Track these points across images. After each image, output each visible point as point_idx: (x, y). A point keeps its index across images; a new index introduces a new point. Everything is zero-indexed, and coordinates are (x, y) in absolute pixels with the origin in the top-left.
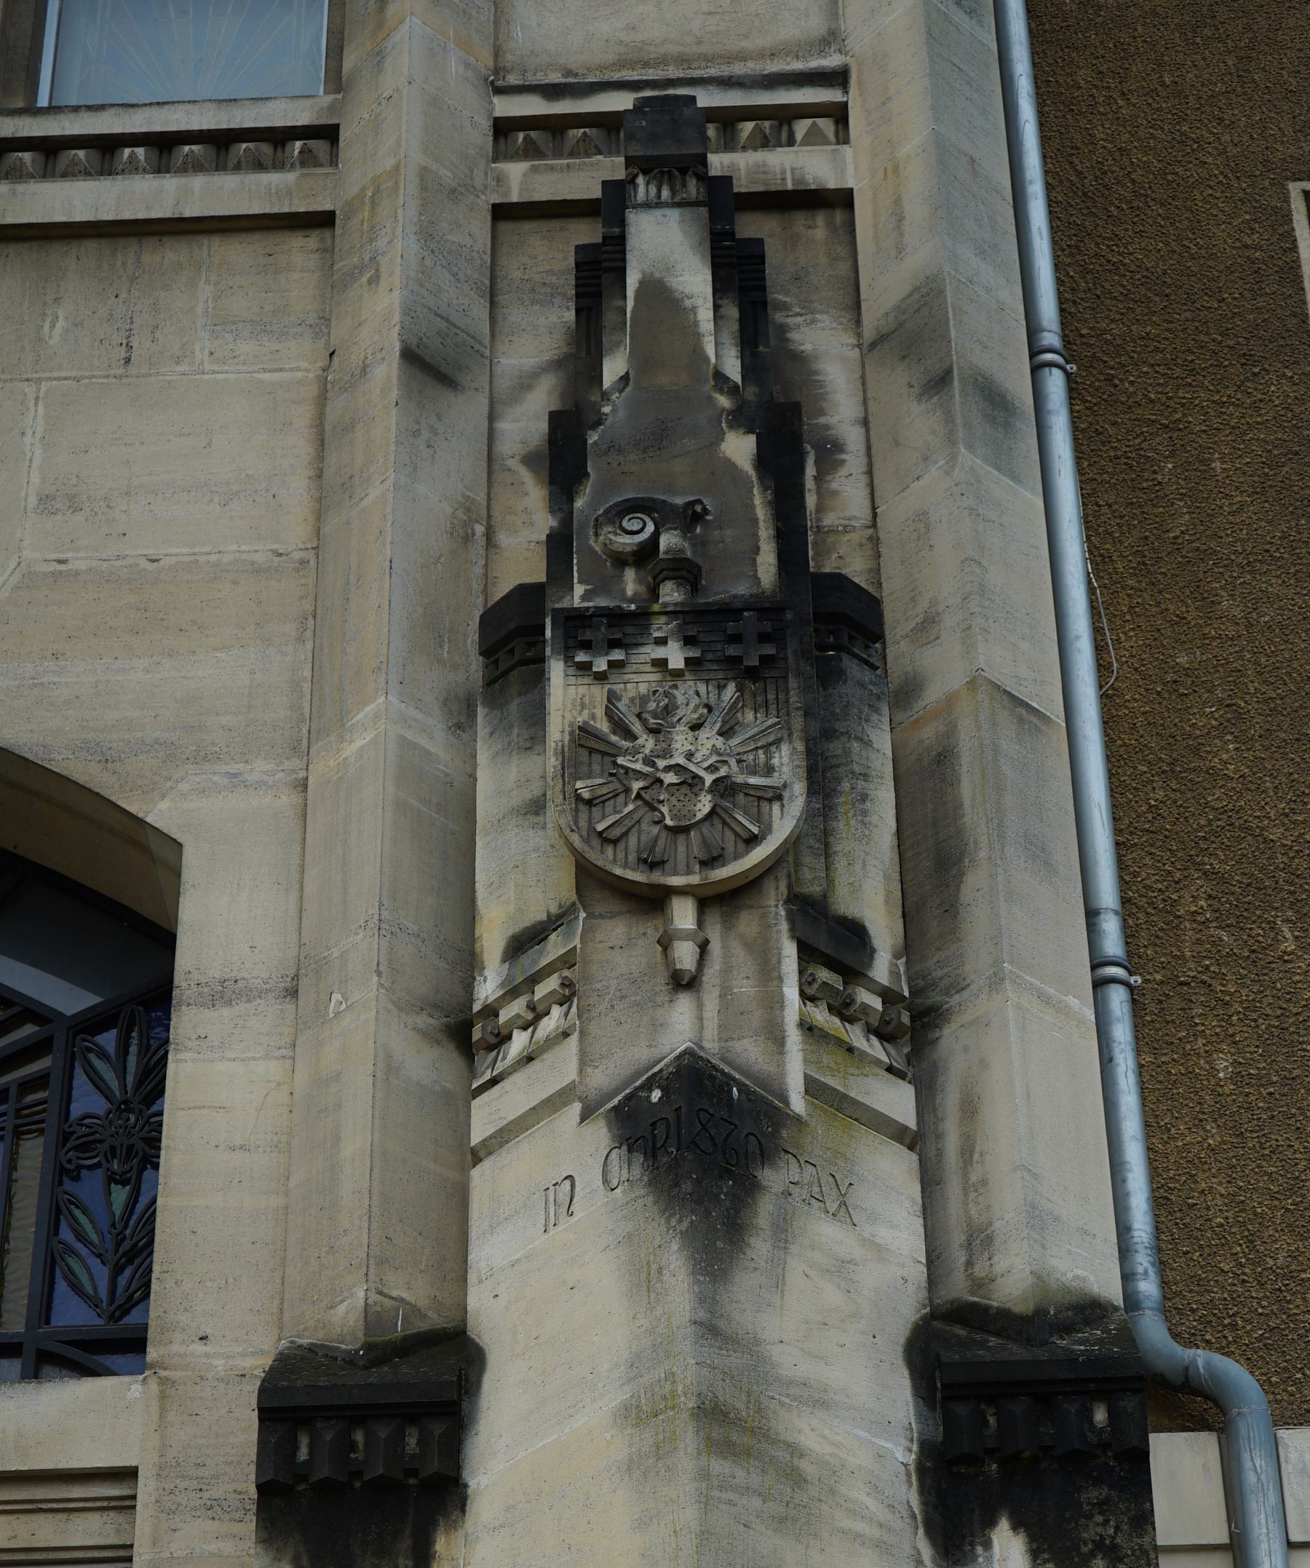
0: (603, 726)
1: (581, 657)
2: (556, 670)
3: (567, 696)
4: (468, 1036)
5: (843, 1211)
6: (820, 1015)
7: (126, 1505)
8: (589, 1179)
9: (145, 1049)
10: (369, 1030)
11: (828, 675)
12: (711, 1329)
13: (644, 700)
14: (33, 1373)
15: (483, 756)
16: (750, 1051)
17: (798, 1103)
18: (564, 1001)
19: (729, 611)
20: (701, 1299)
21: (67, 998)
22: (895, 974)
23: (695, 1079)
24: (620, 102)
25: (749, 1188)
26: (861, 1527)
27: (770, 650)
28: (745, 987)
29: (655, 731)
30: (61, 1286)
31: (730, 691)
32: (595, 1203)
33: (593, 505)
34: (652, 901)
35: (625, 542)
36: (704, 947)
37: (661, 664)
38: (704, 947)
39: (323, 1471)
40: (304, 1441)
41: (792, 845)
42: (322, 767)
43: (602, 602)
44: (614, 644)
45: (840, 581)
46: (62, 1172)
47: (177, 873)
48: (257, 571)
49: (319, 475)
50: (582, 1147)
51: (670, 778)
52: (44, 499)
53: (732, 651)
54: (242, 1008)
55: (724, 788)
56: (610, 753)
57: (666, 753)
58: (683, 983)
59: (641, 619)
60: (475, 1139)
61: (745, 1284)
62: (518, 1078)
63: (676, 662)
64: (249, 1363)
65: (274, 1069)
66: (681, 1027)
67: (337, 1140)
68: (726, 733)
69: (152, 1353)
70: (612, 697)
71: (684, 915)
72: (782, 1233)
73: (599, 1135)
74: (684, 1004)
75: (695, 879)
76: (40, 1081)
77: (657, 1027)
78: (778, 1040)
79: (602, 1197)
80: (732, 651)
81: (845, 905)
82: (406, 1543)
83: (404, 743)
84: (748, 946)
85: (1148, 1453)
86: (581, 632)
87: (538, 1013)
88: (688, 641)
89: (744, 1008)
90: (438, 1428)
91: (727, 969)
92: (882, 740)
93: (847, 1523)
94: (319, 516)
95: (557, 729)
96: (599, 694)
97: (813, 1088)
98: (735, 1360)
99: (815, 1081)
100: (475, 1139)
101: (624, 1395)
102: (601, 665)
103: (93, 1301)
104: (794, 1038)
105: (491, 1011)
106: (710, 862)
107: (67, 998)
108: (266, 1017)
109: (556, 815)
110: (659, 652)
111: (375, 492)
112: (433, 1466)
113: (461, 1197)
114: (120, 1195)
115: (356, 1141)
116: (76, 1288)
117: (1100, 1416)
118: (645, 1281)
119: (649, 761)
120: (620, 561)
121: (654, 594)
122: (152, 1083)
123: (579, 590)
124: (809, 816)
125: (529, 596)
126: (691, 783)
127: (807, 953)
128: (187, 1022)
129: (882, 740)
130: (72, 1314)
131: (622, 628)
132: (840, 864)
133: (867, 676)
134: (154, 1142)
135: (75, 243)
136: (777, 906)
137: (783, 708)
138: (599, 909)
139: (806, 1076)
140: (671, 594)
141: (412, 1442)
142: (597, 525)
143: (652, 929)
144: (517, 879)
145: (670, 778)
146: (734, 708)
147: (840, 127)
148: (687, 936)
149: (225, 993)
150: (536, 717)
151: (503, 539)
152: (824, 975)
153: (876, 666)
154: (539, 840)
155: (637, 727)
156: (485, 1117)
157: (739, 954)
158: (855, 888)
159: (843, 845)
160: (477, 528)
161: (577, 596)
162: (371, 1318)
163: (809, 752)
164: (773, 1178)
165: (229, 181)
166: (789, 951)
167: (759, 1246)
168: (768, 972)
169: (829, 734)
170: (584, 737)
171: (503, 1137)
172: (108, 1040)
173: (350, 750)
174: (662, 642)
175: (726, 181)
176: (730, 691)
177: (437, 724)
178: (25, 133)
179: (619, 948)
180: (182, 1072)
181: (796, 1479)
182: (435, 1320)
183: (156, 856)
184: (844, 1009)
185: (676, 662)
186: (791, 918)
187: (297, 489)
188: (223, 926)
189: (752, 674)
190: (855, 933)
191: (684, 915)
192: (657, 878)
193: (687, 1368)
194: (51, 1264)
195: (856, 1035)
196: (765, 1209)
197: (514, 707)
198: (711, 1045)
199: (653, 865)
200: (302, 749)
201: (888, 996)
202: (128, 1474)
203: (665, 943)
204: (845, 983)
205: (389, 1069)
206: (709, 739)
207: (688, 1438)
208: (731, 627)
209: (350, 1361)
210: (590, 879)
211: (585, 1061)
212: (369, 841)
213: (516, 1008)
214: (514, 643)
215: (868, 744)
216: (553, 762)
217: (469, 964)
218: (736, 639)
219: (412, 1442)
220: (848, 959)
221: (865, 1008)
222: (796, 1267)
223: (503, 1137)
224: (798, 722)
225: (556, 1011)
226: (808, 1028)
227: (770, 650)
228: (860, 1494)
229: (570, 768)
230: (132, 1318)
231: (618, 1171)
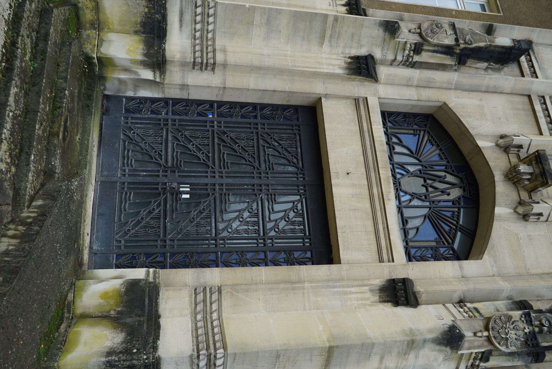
0: (513, 320)
1: (523, 316)
2: (520, 312)
3: (517, 314)
4: (461, 302)
5: (445, 360)
6: (474, 355)
7: (389, 261)
8: (444, 322)
9: (451, 257)
10: (460, 289)
11: (528, 354)
12: (425, 341)
13: (518, 326)
14: (405, 247)
15: (504, 302)
16: (466, 345)
17: (460, 352)
18: (469, 316)
19: (536, 339)
20: (429, 339)
21: (456, 246)
22: (482, 366)
23: (461, 337)
25: (446, 346)
26: (399, 364)
27: (531, 345)
28: (476, 344)
29: (514, 328)
30: (416, 249)
31: (523, 339)
32: (441, 323)
33: (549, 316)
34: (487, 329)
35: (544, 322)
36: (481, 337)
37: (525, 328)
38: (481, 337)
39: (397, 287)
41: (500, 350)
42: (498, 279)
43: (533, 319)
44: (526, 321)
45: (545, 356)
46: (432, 248)
47: (477, 259)
48: (525, 266)
49: (543, 274)
50: (448, 321)
51: (507, 331)
52: (530, 235)
53: (529, 339)
54: (459, 270)
55: (507, 339)
56: (509, 321)
57: (510, 330)
58: (475, 334)
59: (532, 325)
60: (446, 305)
61: (432, 346)
62: (456, 310)
63: (526, 331)
64: (410, 275)
65: (451, 275)
66: (468, 334)
67: (443, 285)
68: (516, 339)
69: (410, 263)
70: (518, 321)
71: (486, 334)
72: (440, 351)
73: (450, 323)
74: (472, 334)
75: (491, 335)
76: (444, 244)
77: (468, 330)
78: (469, 349)
79: (441, 324)
80: (529, 339)
81: (491, 358)
82: (389, 299)
83: (503, 290)
84: (483, 344)
86: (528, 315)
87: (466, 313)
88: (529, 332)
90: (405, 302)
91: (478, 341)
92: (519, 363)
93: (400, 362)
94: (536, 275)
95: (511, 313)
96: (518, 319)
97: (462, 355)
98: (421, 345)
100: (446, 305)
101: (414, 329)
102: (523, 319)
103: (415, 254)
104: (470, 351)
105: (465, 306)
106: (494, 337)
107: (456, 246)
108: (458, 273)
109: (497, 314)
110: (527, 328)
111: (542, 282)
112: (400, 302)
113: (437, 303)
114: (430, 256)
115: (444, 288)
116: (416, 251)
118: (430, 331)
119: (509, 327)
120: (540, 321)
121: (536, 327)
122: (446, 259)
123: (534, 315)
124: (505, 352)
125: (531, 307)
126: (507, 334)
127: (483, 353)
128: (456, 263)
129: (519, 363)
130: (413, 251)
131: (530, 322)
132: (498, 357)
133: (530, 361)
134: (438, 260)
136: (16, 230)
137: (522, 348)
138: (484, 321)
140: (537, 329)
141: (403, 299)
142: (545, 317)
143: (482, 329)
144: (486, 308)
145: (507, 331)
146: (520, 340)
148: (482, 334)
149: (461, 268)
150: (512, 309)
151: (539, 302)
152: (480, 356)
153: (531, 362)
154: (493, 311)
155: (514, 325)
156: (450, 306)
157: (481, 342)
158: (494, 360)
159: (501, 357)
160: (540, 298)
161: (533, 315)
162: (419, 292)
163: (515, 352)
164: (448, 349)
166: (483, 350)
167: (438, 347)
168: (479, 347)
169: (519, 355)
170: (510, 318)
171: (447, 309)
172: (451, 252)
173: (501, 282)
174: (528, 328)
176: (523, 339)
177: (507, 294)
179: (479, 324)
180: (449, 262)
181: (405, 354)
182: (420, 301)
183: (479, 255)
184: (475, 359)
185: (526, 331)
186: (488, 350)
187: (540, 271)
188: (470, 266)
189: (526, 343)
190: (487, 360)
191: (486, 334)
192: (491, 330)
193: (419, 338)
194: (419, 248)
195: (471, 361)
196: (443, 348)
197: (512, 306)
198: (466, 339)
199: (492, 329)
200: (499, 275)
201: (478, 366)
202: (393, 261)
203: (480, 331)
205: (455, 292)
206: (514, 336)
207: (409, 338)
208: (533, 339)
209: (413, 290)
210: (488, 320)
211: (461, 320)
212: (487, 286)
213: (467, 310)
214: (523, 305)
215: (518, 361)
216: (506, 313)
217: (472, 302)
218: (532, 340)
219: (403, 299)
220: (483, 359)
221: (476, 362)
222: (435, 353)
223: (447, 309)
224: (520, 350)
225: (467, 315)
226: (471, 353)
227: (531, 345)
228: (404, 363)
229: (505, 315)
230: (413, 259)
231: (445, 326)
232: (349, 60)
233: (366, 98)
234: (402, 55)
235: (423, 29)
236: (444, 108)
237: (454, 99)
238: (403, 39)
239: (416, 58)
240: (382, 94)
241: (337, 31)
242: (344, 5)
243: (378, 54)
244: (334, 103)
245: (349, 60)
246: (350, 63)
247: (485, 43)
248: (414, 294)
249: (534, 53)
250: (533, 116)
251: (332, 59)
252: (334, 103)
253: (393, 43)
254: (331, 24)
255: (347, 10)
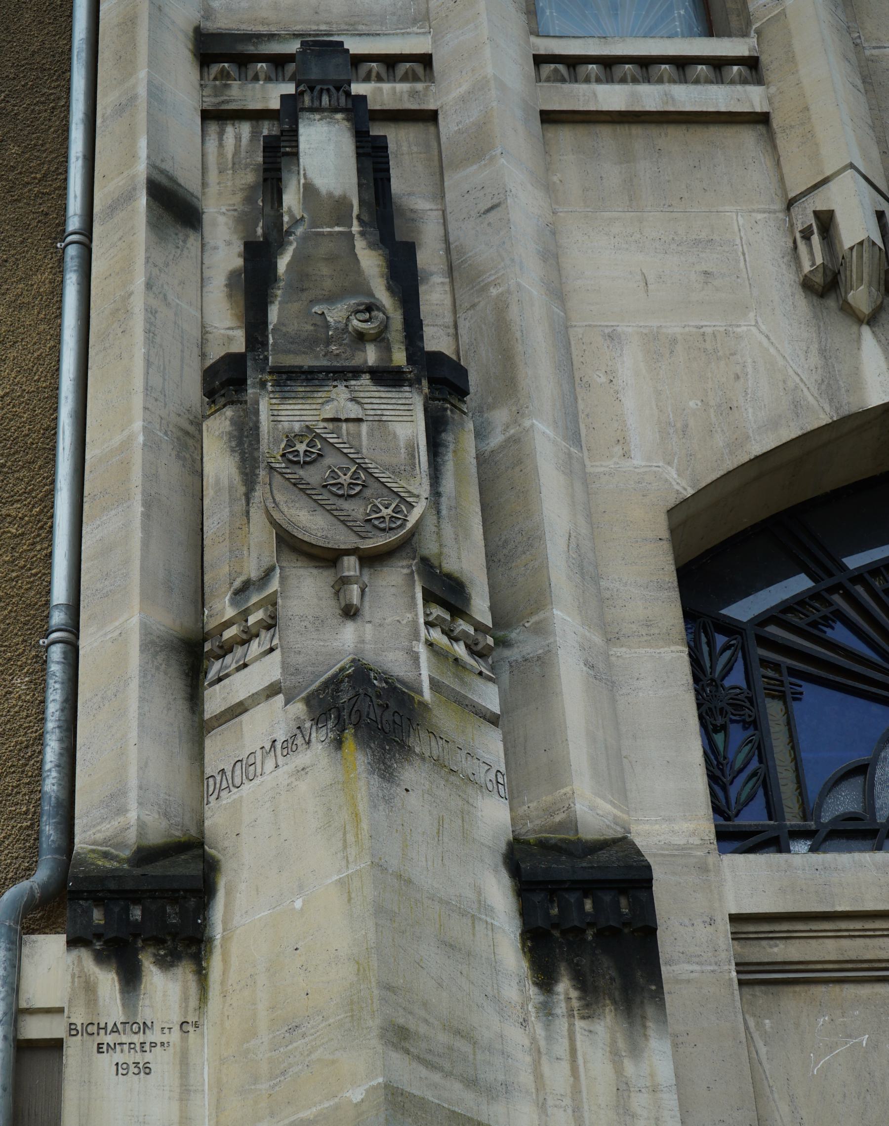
6: (436, 635)
17: (427, 695)
24: (294, 47)
40: (623, 902)
45: (438, 356)
58: (350, 613)
66: (347, 641)
81: (450, 565)
85: (655, 930)
89: (392, 632)
90: (192, 902)
97: (435, 685)
99: (433, 678)
117: (588, 905)
135: (665, 126)
139: (429, 676)
147: (754, 73)
165: (644, 89)
171: (238, 710)
175: (363, 98)
178: (558, 51)
204: (451, 616)
219: (588, 905)
221: (465, 633)
232: (564, 987)
233: (735, 919)
234: (479, 682)
235: (343, 539)
236: (683, 519)
237: (638, 461)
238: (416, 658)
239: (481, 608)
240: (687, 826)
241: (443, 1038)
242: (130, 978)
243: (494, 817)
244: (784, 1108)
245: (564, 987)
246: (582, 983)
247: (360, 244)
248: (147, 855)
249: (271, 37)
250: (654, 131)
251: (576, 1090)
252: (784, 1108)
253: (445, 718)
254: (423, 1071)
255: (166, 963)
